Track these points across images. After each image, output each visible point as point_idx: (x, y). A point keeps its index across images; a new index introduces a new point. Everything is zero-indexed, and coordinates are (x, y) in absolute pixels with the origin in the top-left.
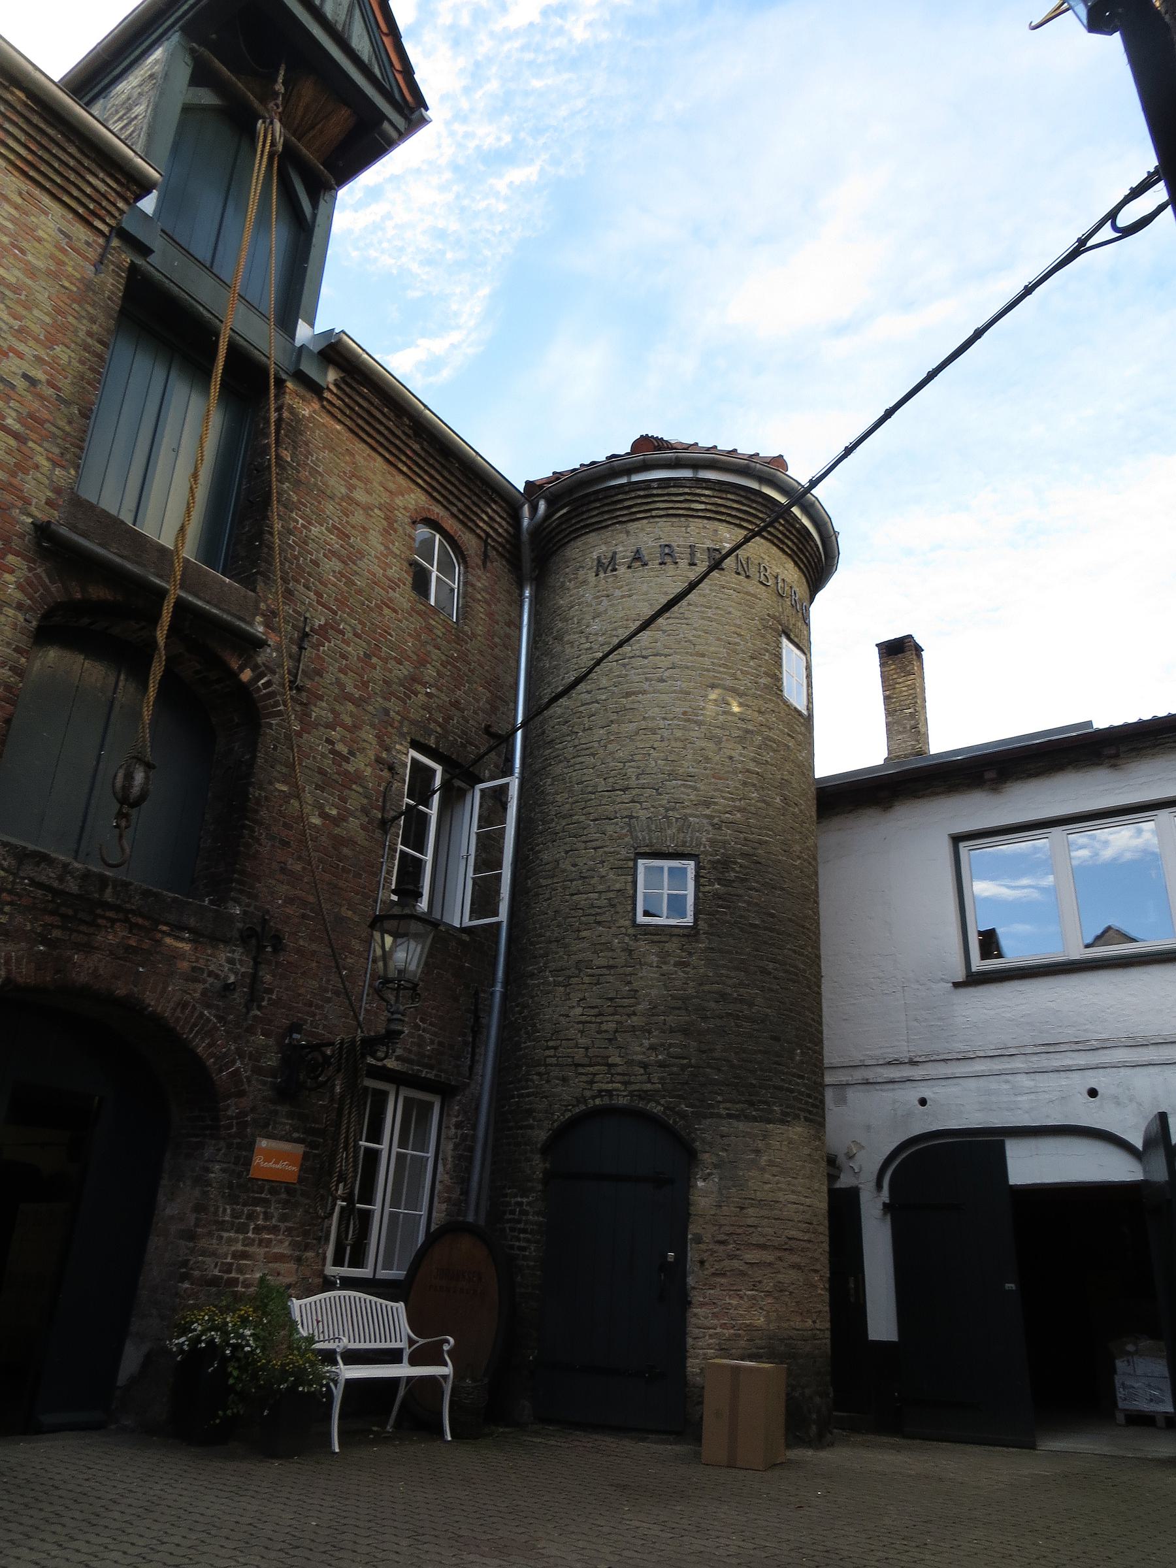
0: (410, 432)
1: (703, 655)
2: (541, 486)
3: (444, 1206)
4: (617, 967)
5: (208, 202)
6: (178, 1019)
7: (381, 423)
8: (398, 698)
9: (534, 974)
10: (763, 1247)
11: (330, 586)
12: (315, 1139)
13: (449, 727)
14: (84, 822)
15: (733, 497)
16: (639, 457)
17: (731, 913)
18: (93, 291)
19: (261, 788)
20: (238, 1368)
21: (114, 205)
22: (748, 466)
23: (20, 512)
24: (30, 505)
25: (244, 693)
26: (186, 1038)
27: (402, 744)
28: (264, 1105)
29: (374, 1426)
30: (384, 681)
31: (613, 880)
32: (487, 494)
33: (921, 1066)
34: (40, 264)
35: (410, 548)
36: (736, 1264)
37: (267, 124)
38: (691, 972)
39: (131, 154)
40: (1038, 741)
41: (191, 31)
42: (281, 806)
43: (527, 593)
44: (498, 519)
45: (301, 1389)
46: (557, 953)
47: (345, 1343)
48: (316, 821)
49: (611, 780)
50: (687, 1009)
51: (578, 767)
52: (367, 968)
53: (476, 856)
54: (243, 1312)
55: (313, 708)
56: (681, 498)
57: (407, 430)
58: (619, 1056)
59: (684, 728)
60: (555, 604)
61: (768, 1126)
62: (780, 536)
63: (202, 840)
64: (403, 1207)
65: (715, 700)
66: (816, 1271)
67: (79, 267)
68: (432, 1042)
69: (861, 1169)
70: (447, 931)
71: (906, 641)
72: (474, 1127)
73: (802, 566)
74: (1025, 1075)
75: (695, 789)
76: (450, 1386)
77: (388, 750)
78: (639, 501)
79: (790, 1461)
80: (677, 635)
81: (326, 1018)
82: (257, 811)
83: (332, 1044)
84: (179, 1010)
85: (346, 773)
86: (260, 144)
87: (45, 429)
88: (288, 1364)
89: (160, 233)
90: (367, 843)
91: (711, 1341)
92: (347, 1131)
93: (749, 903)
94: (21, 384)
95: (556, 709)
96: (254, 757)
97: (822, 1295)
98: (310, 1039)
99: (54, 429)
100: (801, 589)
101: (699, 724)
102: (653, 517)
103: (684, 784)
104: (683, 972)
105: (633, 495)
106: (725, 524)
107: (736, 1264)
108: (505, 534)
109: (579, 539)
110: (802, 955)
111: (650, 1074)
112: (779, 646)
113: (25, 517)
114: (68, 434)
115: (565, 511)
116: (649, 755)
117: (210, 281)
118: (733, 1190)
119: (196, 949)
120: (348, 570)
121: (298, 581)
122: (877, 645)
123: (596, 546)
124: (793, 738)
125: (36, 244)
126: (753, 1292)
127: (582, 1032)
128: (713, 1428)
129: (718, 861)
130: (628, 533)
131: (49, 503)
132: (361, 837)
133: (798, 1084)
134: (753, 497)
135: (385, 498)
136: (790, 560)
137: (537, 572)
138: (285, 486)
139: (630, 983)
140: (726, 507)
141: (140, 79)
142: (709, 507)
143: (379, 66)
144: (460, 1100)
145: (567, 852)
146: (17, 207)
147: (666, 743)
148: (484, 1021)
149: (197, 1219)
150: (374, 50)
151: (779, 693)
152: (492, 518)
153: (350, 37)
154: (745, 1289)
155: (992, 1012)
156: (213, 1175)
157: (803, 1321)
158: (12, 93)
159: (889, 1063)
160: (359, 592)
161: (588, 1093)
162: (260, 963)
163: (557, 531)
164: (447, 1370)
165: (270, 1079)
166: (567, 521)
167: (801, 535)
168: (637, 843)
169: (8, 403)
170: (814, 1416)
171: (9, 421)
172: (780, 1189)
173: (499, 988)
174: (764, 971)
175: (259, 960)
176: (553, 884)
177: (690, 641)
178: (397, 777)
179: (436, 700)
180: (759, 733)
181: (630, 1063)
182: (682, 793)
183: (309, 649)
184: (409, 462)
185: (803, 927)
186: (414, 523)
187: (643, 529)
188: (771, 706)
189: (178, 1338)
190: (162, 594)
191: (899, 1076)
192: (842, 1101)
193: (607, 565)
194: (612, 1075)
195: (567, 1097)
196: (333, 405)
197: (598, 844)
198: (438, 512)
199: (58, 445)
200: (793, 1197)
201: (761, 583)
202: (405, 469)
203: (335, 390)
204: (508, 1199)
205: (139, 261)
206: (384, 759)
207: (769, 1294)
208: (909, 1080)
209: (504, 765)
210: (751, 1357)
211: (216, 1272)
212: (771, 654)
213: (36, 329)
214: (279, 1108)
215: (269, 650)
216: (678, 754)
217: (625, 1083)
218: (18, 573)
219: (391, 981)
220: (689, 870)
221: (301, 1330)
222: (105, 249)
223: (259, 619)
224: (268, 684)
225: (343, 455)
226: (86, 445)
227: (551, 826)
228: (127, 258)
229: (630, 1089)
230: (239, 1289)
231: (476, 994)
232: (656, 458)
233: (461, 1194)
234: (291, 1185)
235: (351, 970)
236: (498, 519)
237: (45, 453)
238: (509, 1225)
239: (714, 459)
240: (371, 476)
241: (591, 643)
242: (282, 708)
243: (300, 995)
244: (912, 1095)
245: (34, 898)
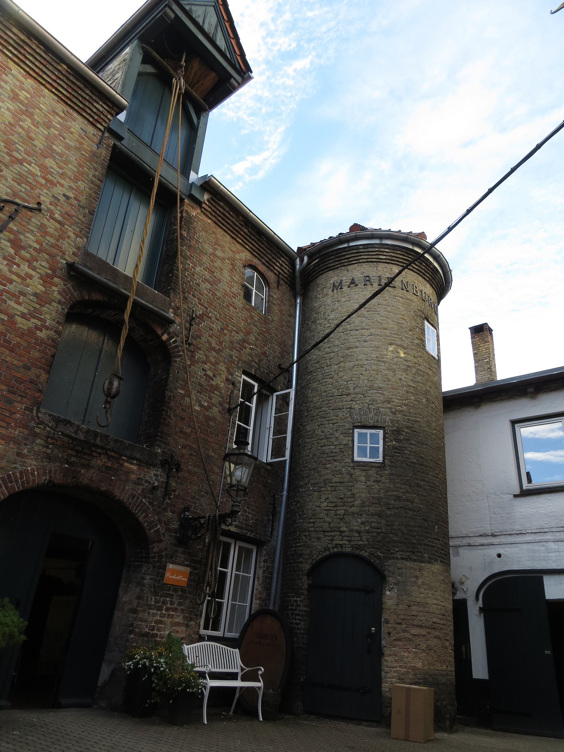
0: (243, 224)
1: (386, 329)
2: (305, 249)
3: (258, 602)
4: (344, 482)
5: (149, 119)
6: (130, 503)
7: (229, 219)
8: (237, 350)
9: (302, 486)
10: (420, 626)
11: (204, 295)
12: (195, 565)
13: (261, 365)
14: (87, 407)
15: (400, 252)
16: (353, 234)
17: (402, 456)
18: (96, 156)
19: (171, 392)
20: (158, 679)
21: (106, 117)
22: (406, 238)
23: (61, 258)
24: (65, 255)
25: (164, 345)
26: (134, 512)
27: (238, 372)
28: (171, 547)
29: (223, 712)
30: (230, 341)
31: (342, 439)
32: (279, 253)
33: (498, 537)
34: (71, 144)
35: (243, 279)
36: (406, 635)
37: (177, 80)
38: (382, 485)
39: (115, 93)
40: (555, 373)
41: (143, 39)
42: (181, 400)
43: (298, 301)
44: (285, 265)
45: (188, 690)
46: (314, 475)
47: (211, 668)
48: (197, 408)
49: (340, 390)
50: (380, 504)
51: (324, 384)
52: (221, 481)
53: (274, 428)
54: (160, 650)
55: (196, 354)
56: (374, 253)
57: (241, 222)
58: (346, 527)
59: (377, 365)
60: (312, 306)
61: (422, 564)
62: (423, 271)
63: (143, 417)
64: (238, 601)
65: (392, 351)
66: (448, 640)
67: (90, 146)
68: (253, 519)
69: (467, 589)
70: (260, 464)
71: (484, 326)
72: (273, 562)
73: (434, 286)
74: (553, 542)
75: (383, 394)
76: (262, 694)
77: (232, 375)
78: (353, 255)
79: (437, 739)
80: (373, 319)
81: (201, 505)
82: (169, 403)
83: (205, 517)
84: (131, 499)
85: (212, 385)
86: (174, 89)
87: (73, 219)
88: (182, 677)
89: (127, 130)
90: (221, 419)
91: (394, 674)
92: (212, 561)
93: (410, 451)
94: (62, 199)
95: (315, 353)
96: (168, 377)
97: (451, 653)
98: (194, 515)
99: (77, 220)
100: (434, 298)
101: (384, 362)
102: (360, 263)
103: (377, 392)
104: (378, 485)
105: (350, 252)
106: (396, 266)
107: (406, 635)
108: (288, 273)
109: (323, 274)
110: (437, 478)
111: (362, 536)
112: (423, 324)
113: (62, 260)
114: (83, 222)
115: (317, 261)
116: (360, 378)
117: (150, 153)
118: (405, 597)
119: (139, 468)
120: (213, 288)
121: (190, 293)
122: (469, 328)
123: (332, 277)
124: (431, 370)
125: (71, 135)
126: (416, 650)
127: (327, 515)
128: (397, 719)
129: (395, 430)
130: (348, 270)
131: (74, 254)
132: (219, 417)
133: (436, 543)
134: (409, 252)
135: (231, 254)
136: (428, 283)
137: (303, 291)
138: (184, 248)
139: (351, 490)
140: (396, 257)
141: (119, 62)
142: (388, 257)
143: (229, 52)
144: (266, 549)
145: (319, 426)
146: (62, 118)
147: (368, 372)
148: (278, 509)
149: (138, 603)
150: (227, 45)
151: (424, 348)
152: (282, 265)
153: (216, 40)
154: (411, 648)
155: (534, 510)
156: (146, 581)
157: (441, 666)
158: (61, 66)
159: (481, 535)
160: (219, 298)
161: (330, 546)
162: (170, 477)
163: (313, 271)
164: (260, 684)
165: (174, 535)
166: (317, 266)
167: (434, 271)
168: (354, 421)
169: (56, 207)
170: (448, 716)
171: (56, 216)
172: (429, 597)
173: (285, 493)
174: (418, 485)
175: (169, 475)
176: (312, 441)
177: (379, 322)
178: (236, 388)
179: (255, 351)
180: (414, 367)
181: (351, 531)
182: (376, 396)
183: (195, 325)
184: (242, 238)
185: (438, 464)
186: (244, 266)
187: (355, 269)
188: (420, 354)
189: (128, 662)
190: (127, 298)
191: (486, 542)
192: (457, 554)
193: (338, 286)
194: (343, 537)
195: (319, 548)
196: (207, 210)
197: (335, 421)
198: (256, 262)
199: (79, 227)
200: (435, 601)
201: (414, 294)
202: (240, 241)
203: (208, 203)
204: (290, 599)
205: (118, 143)
206: (230, 379)
207: (423, 651)
208: (491, 544)
209: (288, 384)
210: (415, 684)
211: (147, 630)
212: (420, 329)
213: (70, 173)
214: (178, 549)
215: (175, 325)
216: (374, 377)
217: (349, 541)
218: (59, 287)
219: (233, 486)
220: (380, 434)
221: (188, 660)
222: (102, 137)
223: (171, 310)
224: (175, 342)
225: (211, 234)
226: (92, 227)
227: (311, 413)
228: (112, 142)
229: (351, 544)
230: (158, 639)
231: (274, 495)
232: (362, 234)
233: (266, 596)
234: (184, 588)
235: (213, 482)
236: (285, 265)
237: (72, 231)
238: (290, 612)
239: (390, 234)
240: (224, 244)
241: (330, 324)
242: (181, 353)
243: (189, 493)
244: (493, 552)
245: (63, 441)
